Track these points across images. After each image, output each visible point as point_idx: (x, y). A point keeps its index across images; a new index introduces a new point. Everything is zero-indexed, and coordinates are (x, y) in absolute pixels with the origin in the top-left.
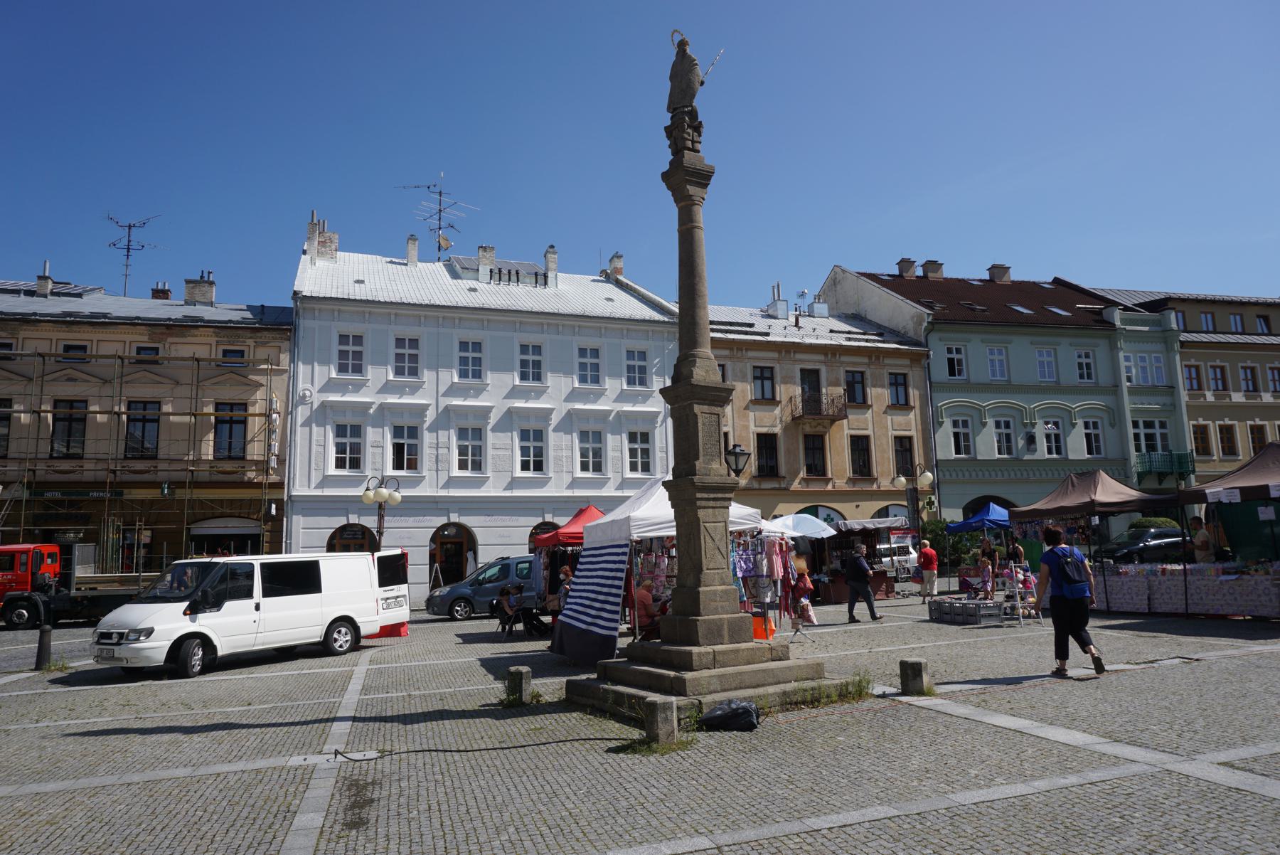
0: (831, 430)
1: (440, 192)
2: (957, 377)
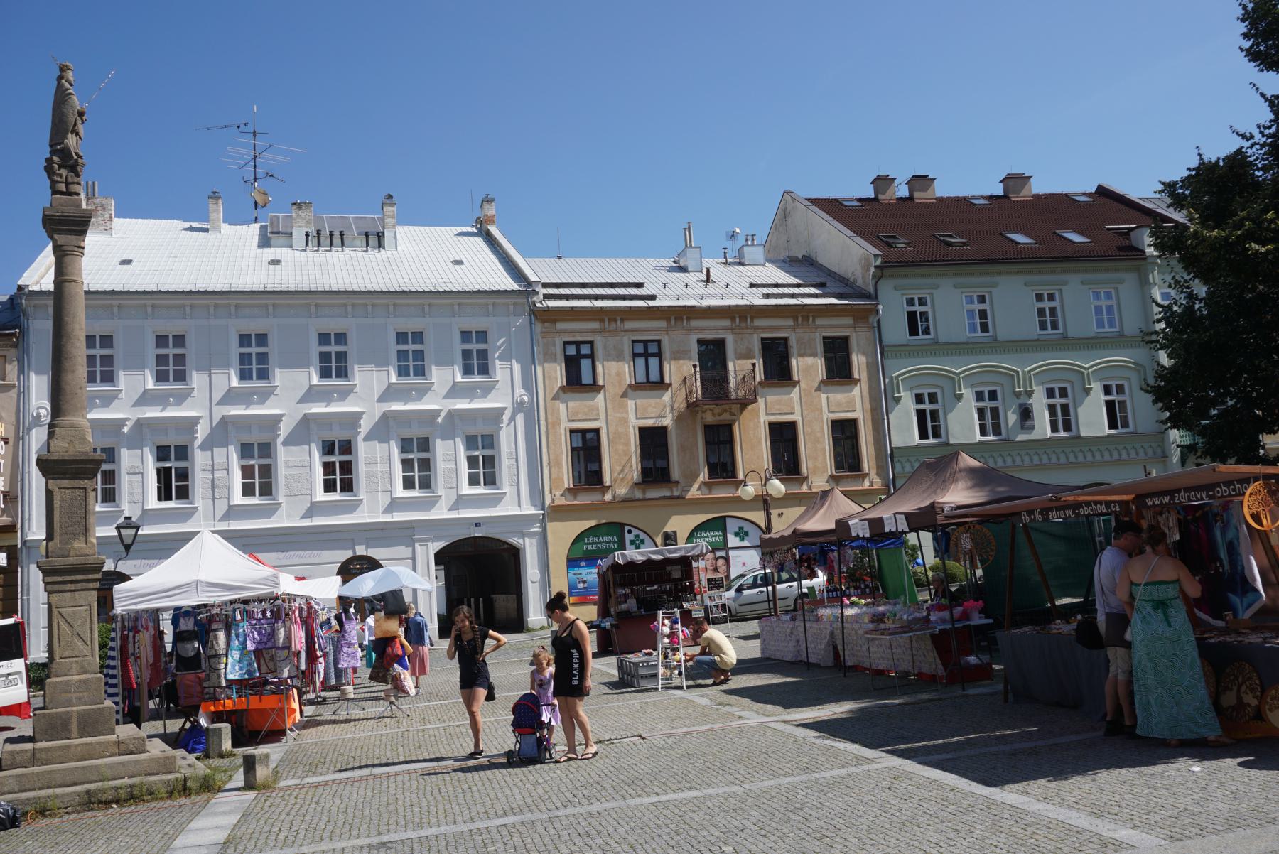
0: (741, 418)
1: (254, 132)
2: (921, 337)
